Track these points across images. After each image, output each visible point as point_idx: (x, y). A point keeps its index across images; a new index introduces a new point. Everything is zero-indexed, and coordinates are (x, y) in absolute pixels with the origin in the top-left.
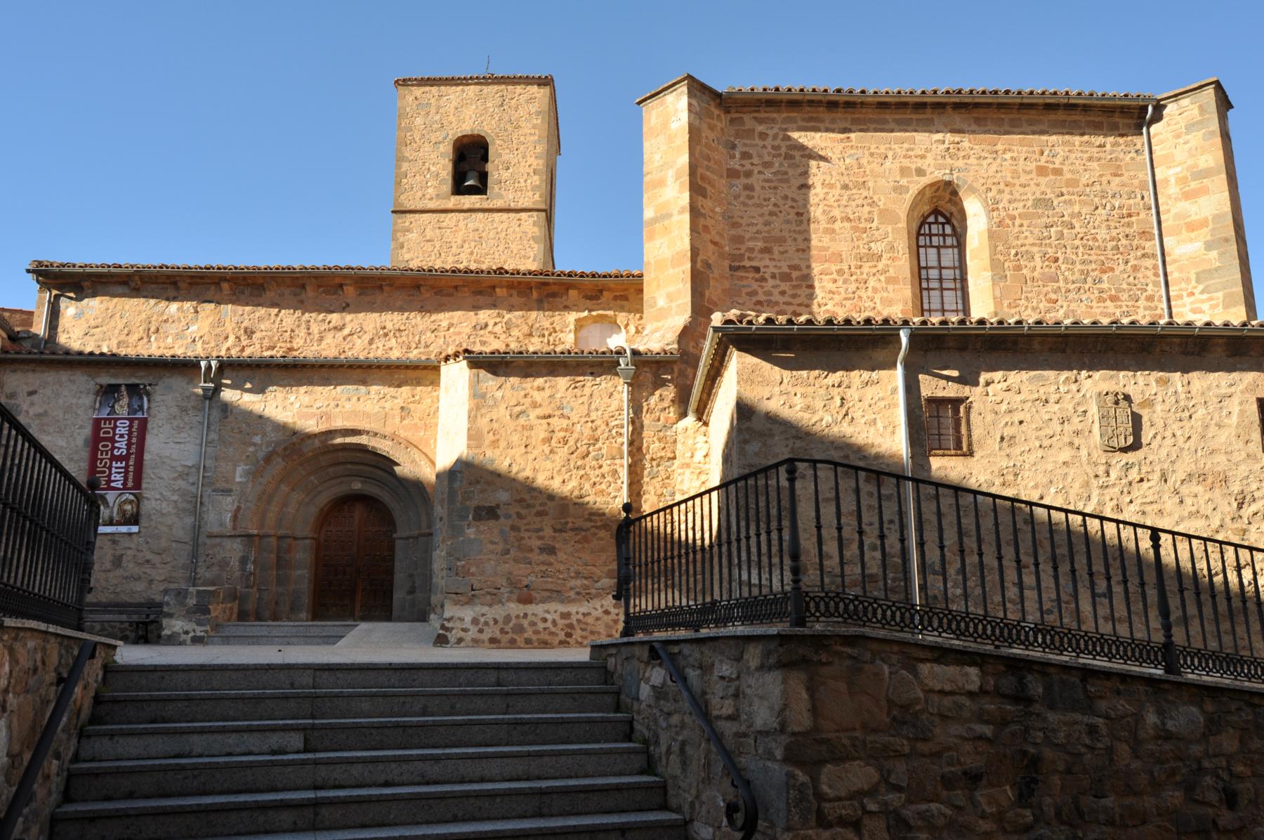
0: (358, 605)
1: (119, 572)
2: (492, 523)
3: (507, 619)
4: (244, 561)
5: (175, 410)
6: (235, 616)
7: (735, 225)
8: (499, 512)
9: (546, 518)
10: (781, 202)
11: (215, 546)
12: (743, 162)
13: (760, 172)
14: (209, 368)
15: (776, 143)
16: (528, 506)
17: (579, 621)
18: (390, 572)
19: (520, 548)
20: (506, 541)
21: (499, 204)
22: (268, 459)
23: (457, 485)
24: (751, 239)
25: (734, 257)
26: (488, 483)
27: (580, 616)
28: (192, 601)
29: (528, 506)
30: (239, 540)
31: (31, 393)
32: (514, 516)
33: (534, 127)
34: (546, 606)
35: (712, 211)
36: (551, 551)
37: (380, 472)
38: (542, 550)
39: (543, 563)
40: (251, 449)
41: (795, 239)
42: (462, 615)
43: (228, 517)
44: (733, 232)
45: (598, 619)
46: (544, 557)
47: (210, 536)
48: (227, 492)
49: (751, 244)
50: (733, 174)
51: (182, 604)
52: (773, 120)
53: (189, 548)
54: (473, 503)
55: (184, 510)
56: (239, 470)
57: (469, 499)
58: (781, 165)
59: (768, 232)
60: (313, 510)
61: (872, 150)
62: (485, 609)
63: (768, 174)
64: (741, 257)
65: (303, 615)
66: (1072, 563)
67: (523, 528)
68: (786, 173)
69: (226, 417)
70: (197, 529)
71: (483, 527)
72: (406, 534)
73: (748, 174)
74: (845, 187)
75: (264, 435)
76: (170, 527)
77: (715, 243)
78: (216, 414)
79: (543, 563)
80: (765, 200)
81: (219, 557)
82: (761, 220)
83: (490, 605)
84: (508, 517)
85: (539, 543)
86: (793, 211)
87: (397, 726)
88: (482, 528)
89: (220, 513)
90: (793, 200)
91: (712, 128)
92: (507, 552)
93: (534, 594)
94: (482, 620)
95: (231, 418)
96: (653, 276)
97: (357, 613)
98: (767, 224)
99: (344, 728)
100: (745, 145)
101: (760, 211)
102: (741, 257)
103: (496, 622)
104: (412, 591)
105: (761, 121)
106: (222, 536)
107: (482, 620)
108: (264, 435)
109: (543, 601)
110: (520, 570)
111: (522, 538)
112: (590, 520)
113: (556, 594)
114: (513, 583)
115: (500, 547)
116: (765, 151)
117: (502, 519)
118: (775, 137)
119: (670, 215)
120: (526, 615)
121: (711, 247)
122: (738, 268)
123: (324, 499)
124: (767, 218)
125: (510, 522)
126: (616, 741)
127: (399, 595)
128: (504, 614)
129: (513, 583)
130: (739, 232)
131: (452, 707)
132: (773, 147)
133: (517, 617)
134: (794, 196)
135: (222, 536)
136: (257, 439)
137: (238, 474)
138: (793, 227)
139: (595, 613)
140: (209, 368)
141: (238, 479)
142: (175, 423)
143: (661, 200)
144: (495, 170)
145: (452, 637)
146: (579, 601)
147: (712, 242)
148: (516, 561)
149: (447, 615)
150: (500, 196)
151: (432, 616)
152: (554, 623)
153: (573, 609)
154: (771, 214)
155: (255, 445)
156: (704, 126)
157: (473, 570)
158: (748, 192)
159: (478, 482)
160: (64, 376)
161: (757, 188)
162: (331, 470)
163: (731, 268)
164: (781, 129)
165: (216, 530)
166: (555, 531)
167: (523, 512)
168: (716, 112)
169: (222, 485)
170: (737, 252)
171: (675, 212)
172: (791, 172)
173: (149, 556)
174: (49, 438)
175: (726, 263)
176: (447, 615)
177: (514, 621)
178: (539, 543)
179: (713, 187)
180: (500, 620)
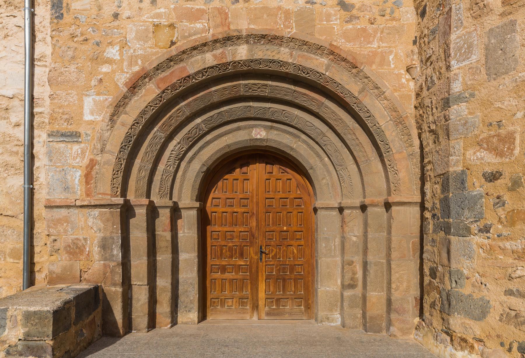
11: (59, 221)
22: (134, 87)
30: (96, 212)
40: (105, 69)
47: (49, 207)
48: (73, 136)
56: (89, 102)
69: (60, 17)
75: (124, 45)
81: (70, 238)
95: (68, 18)
108: (124, 45)
136: (113, 52)
141: (88, 117)
155: (109, 61)
165: (59, 197)
169: (64, 127)
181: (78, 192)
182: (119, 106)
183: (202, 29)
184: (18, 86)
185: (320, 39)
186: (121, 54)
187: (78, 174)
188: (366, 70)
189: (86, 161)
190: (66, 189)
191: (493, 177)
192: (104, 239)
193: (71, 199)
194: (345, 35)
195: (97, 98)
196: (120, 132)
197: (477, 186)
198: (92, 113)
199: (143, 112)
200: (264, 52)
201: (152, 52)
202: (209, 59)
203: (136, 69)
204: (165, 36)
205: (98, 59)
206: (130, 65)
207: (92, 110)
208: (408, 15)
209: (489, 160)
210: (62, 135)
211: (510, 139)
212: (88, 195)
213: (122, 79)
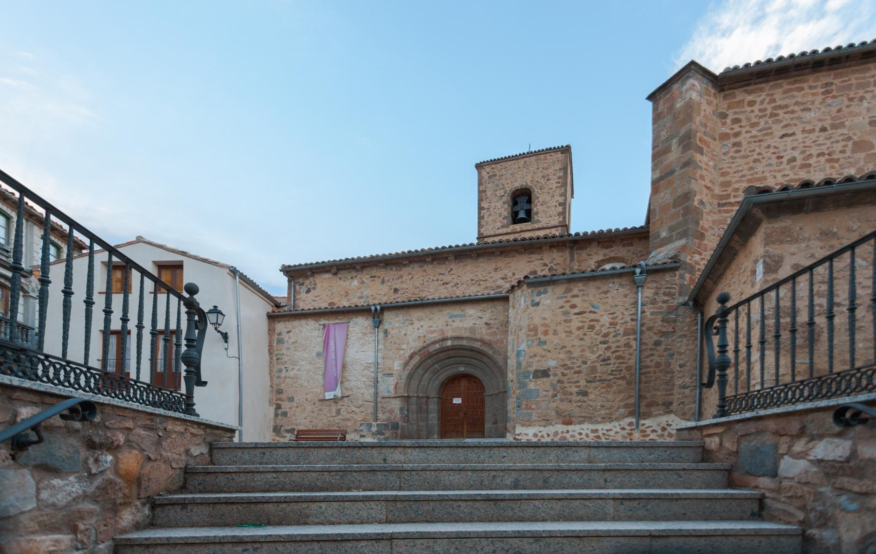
0: (465, 430)
1: (340, 417)
2: (545, 379)
3: (556, 433)
4: (401, 410)
5: (360, 335)
7: (724, 174)
8: (551, 373)
9: (581, 375)
10: (764, 151)
12: (733, 126)
13: (747, 132)
14: (376, 309)
15: (763, 107)
16: (569, 368)
17: (604, 434)
18: (483, 413)
19: (565, 393)
20: (554, 390)
21: (537, 226)
22: (411, 357)
23: (521, 359)
24: (738, 182)
25: (721, 197)
26: (542, 356)
27: (605, 432)
28: (374, 429)
29: (569, 368)
31: (289, 332)
32: (560, 375)
33: (559, 178)
34: (582, 426)
35: (707, 164)
36: (585, 394)
37: (474, 361)
38: (578, 393)
39: (579, 401)
40: (402, 352)
41: (775, 177)
42: (527, 432)
43: (392, 388)
44: (722, 179)
45: (617, 433)
46: (580, 398)
47: (383, 398)
48: (391, 375)
49: (736, 186)
50: (724, 137)
51: (369, 430)
52: (762, 90)
53: (372, 404)
54: (532, 369)
55: (369, 385)
56: (396, 364)
57: (530, 366)
58: (767, 122)
59: (752, 175)
60: (437, 383)
61: (852, 96)
62: (542, 428)
63: (754, 132)
64: (728, 196)
65: (436, 436)
67: (566, 381)
68: (770, 128)
70: (376, 394)
71: (539, 382)
73: (737, 134)
74: (823, 129)
76: (363, 394)
77: (708, 188)
78: (381, 335)
79: (579, 401)
80: (750, 151)
82: (746, 167)
83: (545, 426)
84: (555, 375)
85: (576, 389)
86: (774, 156)
87: (488, 499)
88: (538, 383)
89: (388, 386)
90: (775, 147)
91: (709, 103)
92: (555, 395)
93: (574, 419)
94: (540, 434)
95: (389, 336)
96: (657, 218)
97: (465, 434)
98: (751, 168)
99: (428, 500)
100: (735, 113)
101: (745, 161)
102: (728, 196)
103: (549, 435)
104: (495, 423)
105: (750, 93)
107: (540, 434)
108: (408, 343)
109: (580, 423)
110: (564, 406)
111: (566, 387)
112: (612, 374)
113: (590, 419)
114: (559, 413)
115: (551, 393)
116: (753, 115)
117: (552, 377)
118: (762, 102)
119: (672, 172)
120: (568, 432)
121: (705, 191)
122: (725, 204)
123: (444, 376)
124: (751, 164)
125: (557, 378)
126: (741, 519)
127: (488, 426)
128: (553, 431)
129: (559, 413)
130: (727, 178)
131: (546, 481)
132: (760, 110)
133: (563, 432)
134: (777, 145)
138: (775, 168)
139: (615, 430)
140: (376, 309)
141: (396, 368)
142: (361, 342)
143: (665, 163)
144: (537, 207)
146: (604, 422)
147: (706, 186)
148: (562, 400)
149: (517, 432)
150: (539, 221)
151: (508, 434)
152: (587, 435)
153: (599, 427)
154: (755, 161)
156: (704, 101)
157: (533, 406)
158: (735, 148)
159: (535, 356)
160: (303, 322)
161: (744, 143)
163: (719, 205)
164: (768, 95)
165: (386, 395)
166: (588, 382)
167: (565, 372)
168: (713, 91)
169: (388, 372)
170: (725, 193)
171: (678, 169)
172: (775, 127)
173: (354, 409)
174: (299, 354)
175: (715, 202)
176: (517, 432)
177: (560, 435)
178: (576, 389)
179: (708, 146)
180: (551, 435)
181: (392, 394)
182: (406, 364)
183: (436, 336)
184: (372, 360)
185: (478, 336)
187: (393, 387)
188: (495, 346)
194: (487, 334)
196: (407, 372)
200: (456, 343)
201: (418, 345)
202: (437, 346)
204: (422, 340)
205: (399, 349)
207: (397, 366)
208: (869, 168)
213: (407, 355)
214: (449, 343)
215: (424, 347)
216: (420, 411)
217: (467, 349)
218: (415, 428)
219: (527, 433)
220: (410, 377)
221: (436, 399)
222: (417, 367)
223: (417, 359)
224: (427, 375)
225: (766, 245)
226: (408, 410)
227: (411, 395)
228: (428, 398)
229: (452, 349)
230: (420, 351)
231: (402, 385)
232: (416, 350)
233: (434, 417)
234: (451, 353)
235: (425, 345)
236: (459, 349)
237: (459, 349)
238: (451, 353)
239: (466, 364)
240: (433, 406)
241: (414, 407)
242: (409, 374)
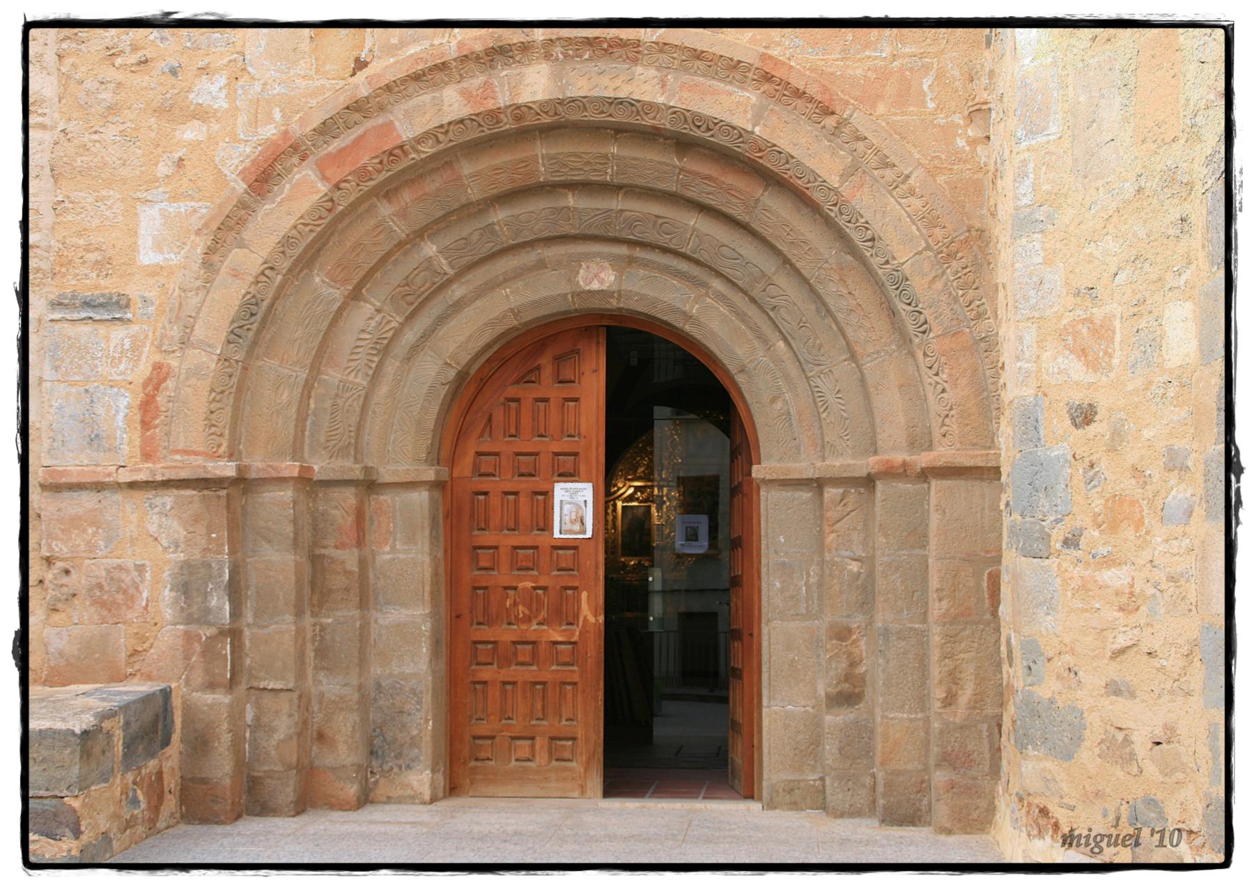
4: (189, 585)
6: (170, 804)
11: (75, 522)
22: (263, 178)
30: (168, 499)
37: (693, 221)
40: (191, 133)
43: (120, 409)
48: (110, 307)
56: (150, 220)
65: (421, 779)
66: (844, 336)
72: (805, 467)
81: (98, 568)
106: (99, 487)
123: (468, 330)
135: (99, 487)
137: (145, 241)
141: (148, 257)
145: (1149, 565)
155: (201, 114)
162: (500, 215)
181: (123, 455)
182: (227, 229)
186: (231, 96)
188: (859, 120)
189: (144, 370)
190: (94, 440)
191: (1084, 416)
192: (187, 566)
193: (106, 469)
195: (172, 208)
196: (229, 295)
197: (1061, 440)
198: (158, 247)
199: (287, 241)
200: (594, 81)
202: (452, 103)
203: (269, 131)
206: (254, 122)
209: (1069, 374)
210: (87, 304)
211: (1102, 331)
212: (147, 456)
213: (235, 159)
214: (535, 84)
215: (358, 107)
216: (316, 586)
217: (651, 136)
218: (284, 726)
219: (314, 748)
220: (255, 325)
221: (421, 497)
222: (306, 253)
223: (303, 191)
224: (365, 310)
225: (441, 252)
226: (235, 590)
227: (258, 465)
228: (370, 485)
229: (551, 131)
230: (326, 129)
231: (192, 396)
232: (301, 128)
233: (405, 637)
234: (542, 158)
235: (361, 85)
236: (597, 130)
237: (597, 130)
238: (542, 158)
239: (635, 245)
240: (406, 551)
241: (277, 562)
242: (250, 306)
